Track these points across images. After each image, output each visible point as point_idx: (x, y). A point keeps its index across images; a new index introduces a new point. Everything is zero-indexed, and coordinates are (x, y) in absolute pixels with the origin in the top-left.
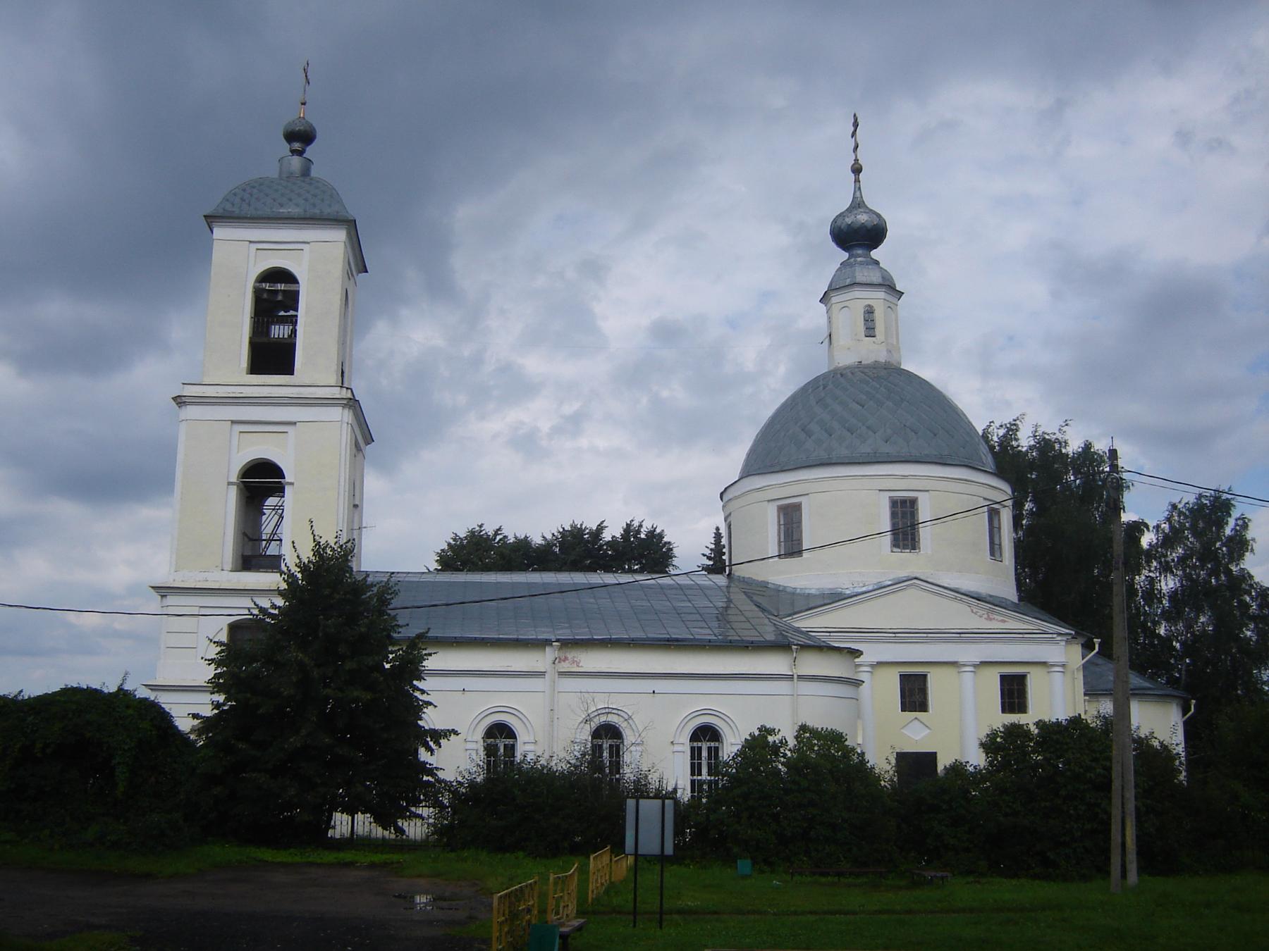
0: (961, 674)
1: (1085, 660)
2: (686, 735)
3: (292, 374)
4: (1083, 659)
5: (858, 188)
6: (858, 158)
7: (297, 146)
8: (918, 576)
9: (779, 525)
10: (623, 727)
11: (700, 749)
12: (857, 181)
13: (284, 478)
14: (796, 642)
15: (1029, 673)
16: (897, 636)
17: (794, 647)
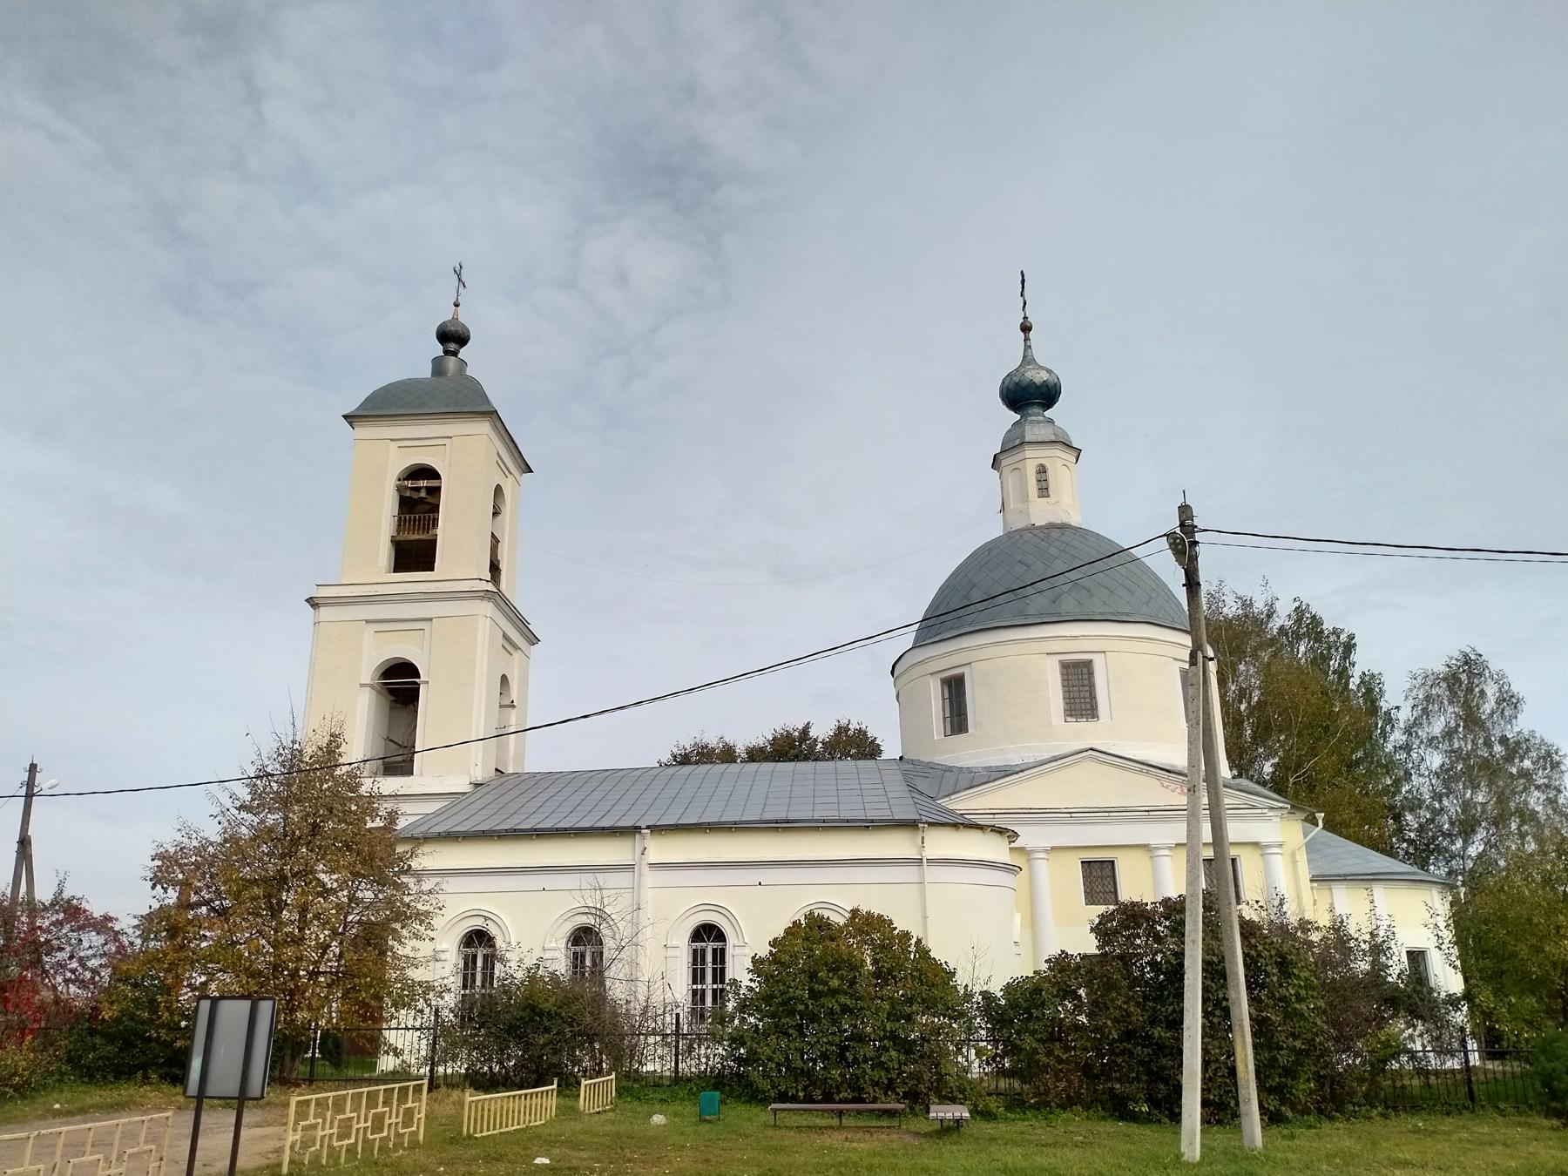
0: (1154, 859)
1: (1307, 839)
2: (455, 936)
3: (433, 570)
4: (1305, 838)
5: (1027, 347)
6: (1027, 315)
7: (452, 346)
8: (1094, 747)
9: (944, 699)
10: (493, 930)
11: (703, 951)
12: (1026, 339)
13: (419, 678)
14: (924, 819)
15: (1239, 856)
16: (1072, 816)
17: (920, 825)
